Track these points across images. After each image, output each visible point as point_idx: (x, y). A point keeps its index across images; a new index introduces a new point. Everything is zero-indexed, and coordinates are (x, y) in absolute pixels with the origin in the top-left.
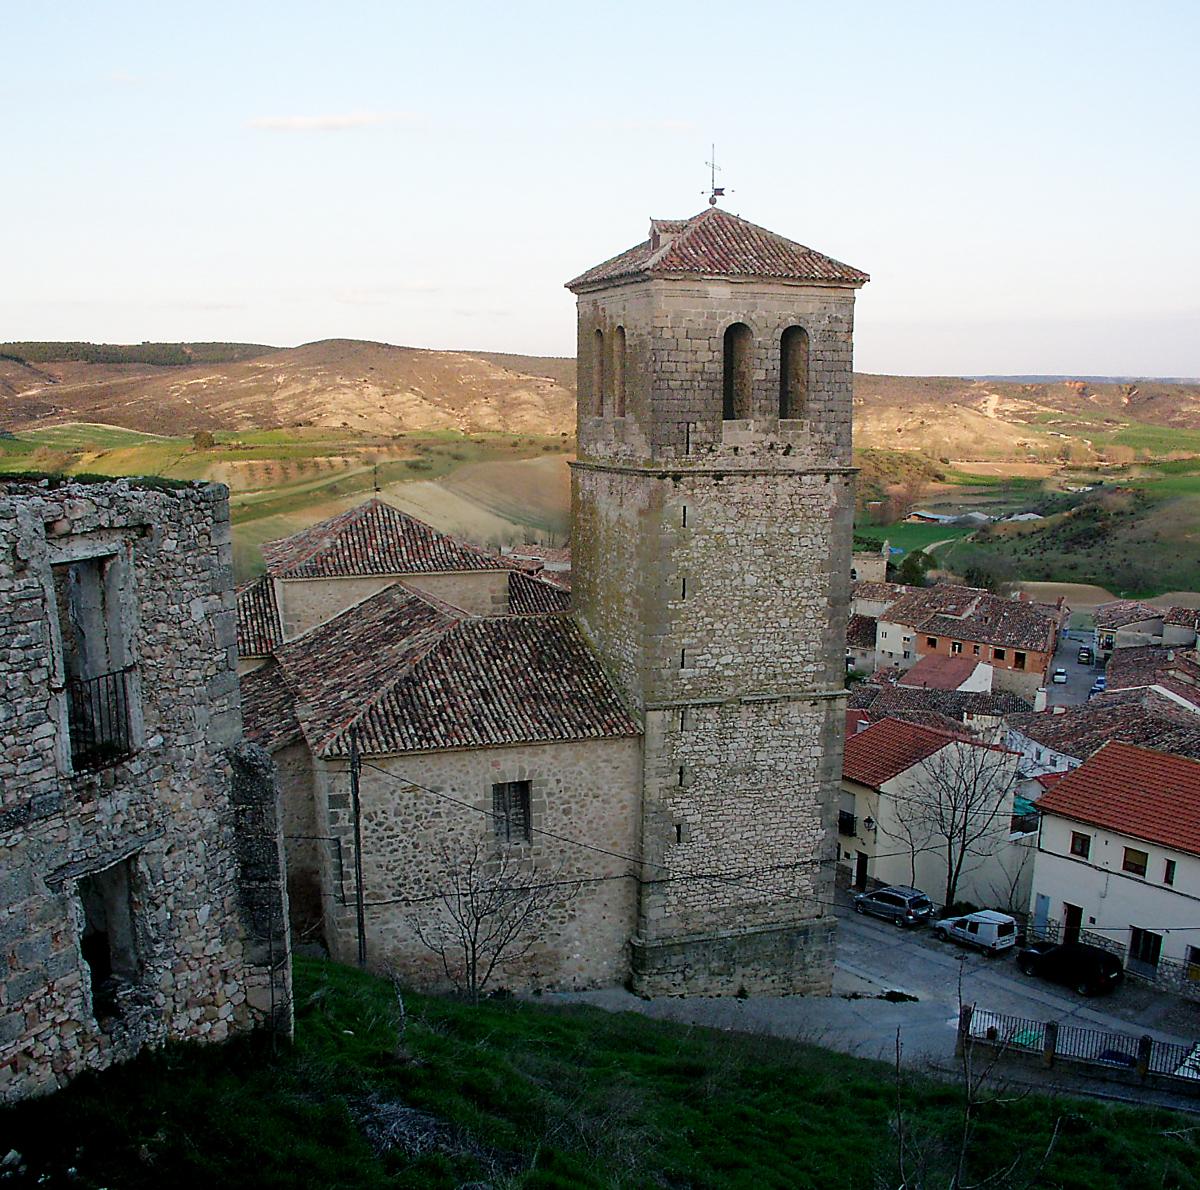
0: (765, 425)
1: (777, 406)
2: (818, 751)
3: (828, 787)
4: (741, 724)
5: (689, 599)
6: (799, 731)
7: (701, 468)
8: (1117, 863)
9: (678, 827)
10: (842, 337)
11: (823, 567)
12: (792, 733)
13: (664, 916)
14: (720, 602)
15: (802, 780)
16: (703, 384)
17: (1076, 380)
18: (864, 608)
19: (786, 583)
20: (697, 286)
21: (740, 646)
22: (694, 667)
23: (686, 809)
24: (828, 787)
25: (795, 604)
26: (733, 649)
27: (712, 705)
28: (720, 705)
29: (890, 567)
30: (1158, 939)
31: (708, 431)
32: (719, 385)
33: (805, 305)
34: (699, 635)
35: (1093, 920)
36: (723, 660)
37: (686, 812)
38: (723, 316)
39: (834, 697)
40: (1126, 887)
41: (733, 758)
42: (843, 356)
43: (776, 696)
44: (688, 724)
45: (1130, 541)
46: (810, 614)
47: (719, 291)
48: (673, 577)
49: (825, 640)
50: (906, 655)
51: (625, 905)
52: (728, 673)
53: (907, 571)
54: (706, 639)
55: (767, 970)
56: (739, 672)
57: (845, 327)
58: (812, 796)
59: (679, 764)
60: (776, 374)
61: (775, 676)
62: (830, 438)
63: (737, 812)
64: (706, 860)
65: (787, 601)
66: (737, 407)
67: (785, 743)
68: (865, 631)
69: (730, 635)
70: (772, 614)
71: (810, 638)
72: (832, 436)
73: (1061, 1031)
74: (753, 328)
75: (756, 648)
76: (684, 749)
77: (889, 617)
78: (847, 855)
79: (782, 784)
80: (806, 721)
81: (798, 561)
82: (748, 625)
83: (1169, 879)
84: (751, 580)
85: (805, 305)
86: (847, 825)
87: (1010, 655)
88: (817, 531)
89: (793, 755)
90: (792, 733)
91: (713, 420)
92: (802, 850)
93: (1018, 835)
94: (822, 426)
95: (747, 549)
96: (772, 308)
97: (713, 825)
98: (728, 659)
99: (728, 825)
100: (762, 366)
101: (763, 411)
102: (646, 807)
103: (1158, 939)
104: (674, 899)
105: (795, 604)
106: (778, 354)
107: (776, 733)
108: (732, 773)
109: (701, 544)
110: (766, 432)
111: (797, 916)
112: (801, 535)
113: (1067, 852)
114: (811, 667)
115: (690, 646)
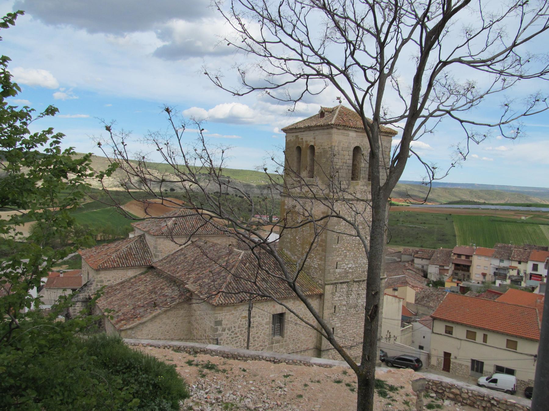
0: (364, 183)
4: (354, 289)
8: (443, 331)
16: (346, 168)
21: (354, 261)
22: (340, 269)
26: (352, 262)
28: (348, 282)
37: (336, 323)
38: (353, 143)
41: (351, 302)
44: (338, 290)
52: (350, 270)
59: (334, 305)
75: (359, 261)
83: (485, 340)
101: (364, 178)
108: (350, 308)
110: (363, 186)
115: (339, 261)
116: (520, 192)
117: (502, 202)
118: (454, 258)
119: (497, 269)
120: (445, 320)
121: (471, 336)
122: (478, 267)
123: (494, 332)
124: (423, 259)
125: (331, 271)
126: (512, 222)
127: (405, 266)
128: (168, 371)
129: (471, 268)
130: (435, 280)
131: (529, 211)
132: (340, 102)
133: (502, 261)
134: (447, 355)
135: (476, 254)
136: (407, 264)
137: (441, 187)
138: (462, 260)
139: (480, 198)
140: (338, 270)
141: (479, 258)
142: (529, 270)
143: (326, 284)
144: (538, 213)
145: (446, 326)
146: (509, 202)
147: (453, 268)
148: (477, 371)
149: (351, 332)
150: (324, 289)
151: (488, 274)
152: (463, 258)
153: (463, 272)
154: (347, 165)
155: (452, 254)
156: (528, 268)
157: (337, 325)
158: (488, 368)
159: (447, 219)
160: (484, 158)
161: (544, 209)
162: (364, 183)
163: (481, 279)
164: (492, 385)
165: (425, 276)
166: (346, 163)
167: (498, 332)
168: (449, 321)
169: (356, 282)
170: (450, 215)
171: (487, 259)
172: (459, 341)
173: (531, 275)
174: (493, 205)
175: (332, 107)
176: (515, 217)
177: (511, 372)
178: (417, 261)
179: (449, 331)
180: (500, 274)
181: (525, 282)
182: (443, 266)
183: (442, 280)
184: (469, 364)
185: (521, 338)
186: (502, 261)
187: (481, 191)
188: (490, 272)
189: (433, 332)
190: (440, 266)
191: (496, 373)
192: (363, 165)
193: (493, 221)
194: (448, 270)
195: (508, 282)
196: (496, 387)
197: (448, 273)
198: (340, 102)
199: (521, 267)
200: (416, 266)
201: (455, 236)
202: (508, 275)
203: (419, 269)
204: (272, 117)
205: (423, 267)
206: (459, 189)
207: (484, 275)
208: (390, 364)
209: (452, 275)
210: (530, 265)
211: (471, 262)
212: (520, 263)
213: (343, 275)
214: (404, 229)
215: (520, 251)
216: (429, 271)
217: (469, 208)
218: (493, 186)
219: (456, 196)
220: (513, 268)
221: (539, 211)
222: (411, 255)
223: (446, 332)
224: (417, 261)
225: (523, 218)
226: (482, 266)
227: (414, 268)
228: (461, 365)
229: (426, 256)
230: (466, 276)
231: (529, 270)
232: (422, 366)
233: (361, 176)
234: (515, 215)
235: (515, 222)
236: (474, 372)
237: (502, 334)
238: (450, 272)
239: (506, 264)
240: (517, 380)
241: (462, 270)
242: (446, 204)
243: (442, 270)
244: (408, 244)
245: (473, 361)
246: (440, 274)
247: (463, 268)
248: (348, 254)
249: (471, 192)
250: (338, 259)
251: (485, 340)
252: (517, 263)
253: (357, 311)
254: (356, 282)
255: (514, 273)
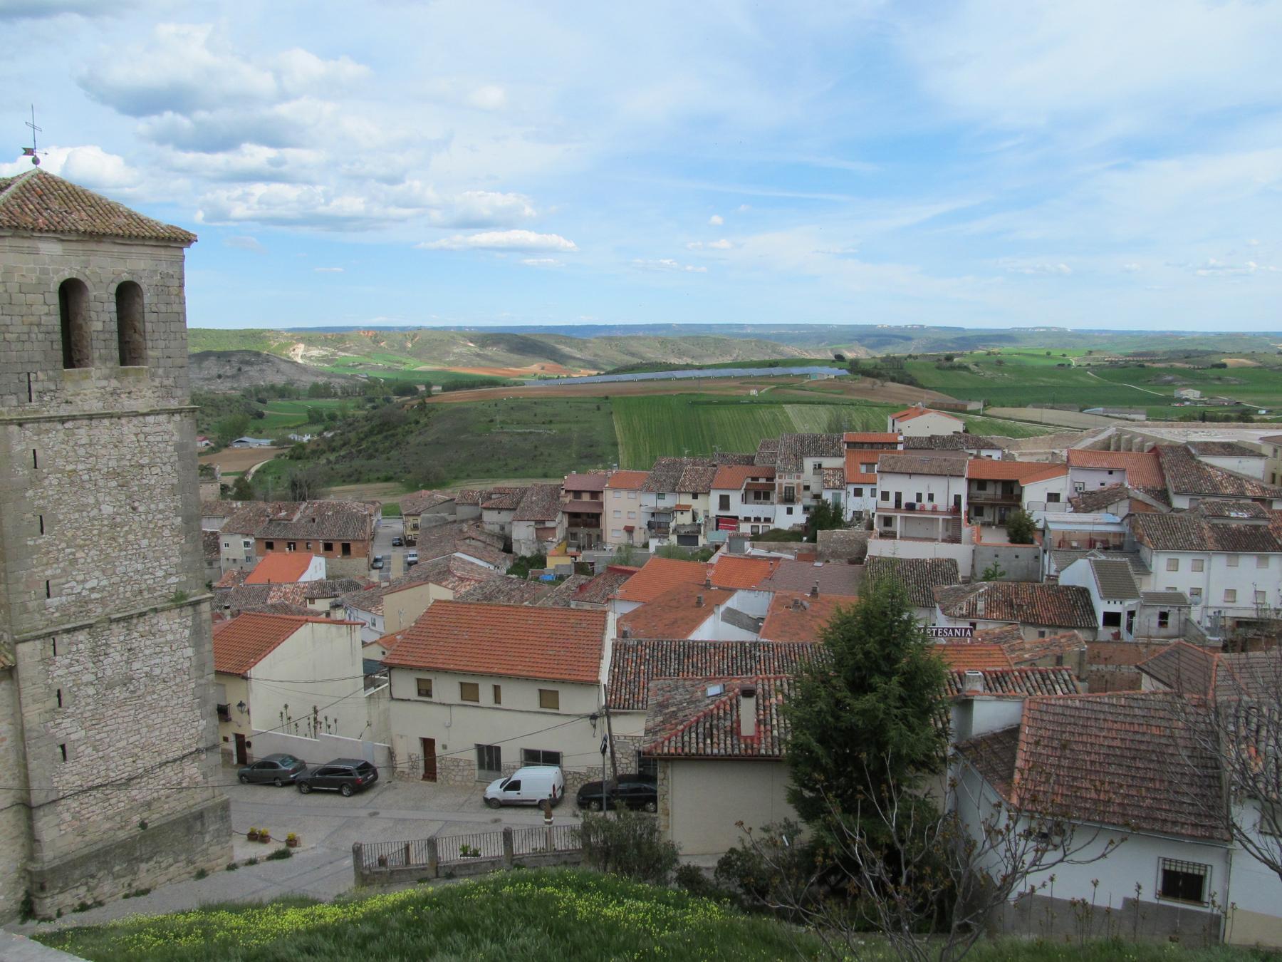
0: (107, 371)
1: (116, 354)
2: (190, 652)
3: (202, 681)
4: (113, 640)
5: (49, 533)
6: (170, 637)
7: (46, 414)
8: (412, 692)
9: (63, 747)
10: (174, 290)
11: (173, 490)
12: (163, 640)
13: (58, 835)
14: (79, 533)
15: (178, 680)
16: (40, 336)
17: (368, 329)
18: (209, 526)
19: (141, 509)
20: (26, 243)
21: (103, 571)
22: (60, 595)
23: (69, 729)
24: (202, 681)
25: (151, 526)
26: (97, 573)
27: (82, 628)
28: (90, 626)
29: (224, 488)
30: (498, 749)
31: (50, 379)
32: (58, 337)
33: (137, 264)
34: (62, 565)
35: (445, 747)
36: (88, 585)
37: (69, 731)
38: (56, 272)
39: (198, 603)
40: (466, 716)
41: (109, 672)
42: (176, 308)
43: (144, 609)
45: (418, 445)
46: (167, 532)
47: (50, 249)
48: (29, 515)
49: (183, 554)
50: (248, 559)
51: (15, 834)
52: (94, 596)
53: (239, 488)
54: (69, 569)
55: (171, 860)
56: (105, 594)
57: (176, 283)
58: (190, 692)
60: (114, 326)
61: (141, 592)
62: (170, 382)
63: (120, 720)
64: (95, 771)
65: (144, 524)
66: (76, 356)
67: (158, 650)
68: (212, 544)
69: (93, 561)
70: (131, 537)
71: (170, 553)
72: (171, 380)
73: (439, 843)
74: (88, 284)
75: (120, 570)
76: (59, 672)
77: (230, 530)
78: (226, 739)
79: (161, 686)
80: (175, 626)
81: (150, 488)
82: (109, 550)
83: (497, 699)
84: (107, 509)
85: (137, 264)
86: (223, 712)
87: (337, 547)
88: (166, 460)
89: (167, 659)
90: (163, 640)
91: (54, 369)
92: (187, 742)
93: (372, 691)
94: (160, 371)
95: (101, 483)
96: (103, 269)
97: (98, 737)
98: (93, 583)
99: (112, 735)
100: (100, 316)
101: (104, 360)
102: (27, 735)
103: (498, 749)
104: (67, 816)
105: (151, 526)
106: (113, 307)
107: (148, 643)
108: (110, 687)
109: (55, 482)
110: (107, 378)
111: (191, 802)
112: (150, 465)
113: (536, 707)
114: (174, 579)
115: (54, 577)
116: (762, 337)
117: (727, 360)
118: (567, 500)
119: (653, 514)
120: (411, 668)
121: (469, 693)
122: (617, 515)
123: (510, 677)
124: (500, 510)
125: (32, 605)
126: (732, 403)
127: (461, 531)
128: (909, 680)
129: (602, 519)
130: (528, 555)
131: (768, 377)
132: (36, 161)
133: (661, 496)
134: (428, 744)
135: (611, 488)
136: (465, 527)
137: (604, 335)
138: (584, 505)
139: (681, 354)
140: (53, 601)
141: (617, 495)
142: (715, 511)
143: (17, 642)
144: (784, 380)
145: (418, 680)
146: (739, 359)
147: (566, 523)
148: (490, 768)
149: (123, 743)
150: (14, 654)
151: (637, 528)
152: (586, 498)
153: (586, 530)
154: (43, 329)
155: (563, 492)
156: (709, 505)
157: (73, 737)
158: (510, 755)
159: (599, 409)
160: (689, 268)
161: (796, 371)
162: (107, 371)
163: (623, 538)
164: (512, 795)
165: (508, 549)
166: (39, 325)
167: (518, 678)
168: (420, 669)
169: (118, 620)
170: (607, 398)
171: (632, 495)
172: (446, 710)
173: (719, 520)
174: (709, 367)
175: (9, 176)
176: (740, 392)
177: (552, 758)
178: (489, 516)
179: (425, 690)
180: (657, 525)
181: (705, 536)
182: (543, 522)
183: (543, 552)
184: (473, 756)
185: (563, 682)
186: (661, 496)
187: (685, 339)
188: (641, 522)
189: (392, 699)
190: (537, 522)
191: (527, 765)
192: (98, 326)
193: (694, 403)
194: (554, 528)
195: (674, 539)
196: (519, 797)
197: (554, 536)
198: (36, 161)
199: (698, 505)
200: (488, 527)
201: (615, 444)
202: (672, 525)
203: (491, 535)
204: (182, 183)
205: (502, 528)
206: (639, 338)
207: (630, 530)
208: (305, 788)
209: (565, 539)
210: (715, 497)
211: (601, 505)
212: (695, 496)
213: (73, 609)
214: (505, 439)
215: (697, 471)
216: (514, 536)
217: (652, 380)
218: (709, 326)
219: (632, 354)
220: (683, 509)
221: (788, 376)
222: (477, 504)
223: (420, 694)
224: (489, 516)
225: (753, 392)
226: (624, 510)
227: (483, 532)
228: (456, 762)
229: (507, 502)
230: (594, 538)
231: (715, 511)
232: (376, 777)
233: (96, 355)
234: (739, 388)
235: (738, 403)
236: (485, 772)
237: (527, 679)
238: (560, 533)
239: (669, 501)
240: (565, 775)
241: (586, 525)
242: (614, 372)
243: (542, 531)
244: (516, 472)
245: (480, 749)
246: (539, 539)
247: (586, 522)
248: (80, 554)
249: (663, 342)
250: (49, 573)
251: (497, 699)
252: (691, 496)
253: (134, 692)
254: (118, 620)
255: (685, 519)
